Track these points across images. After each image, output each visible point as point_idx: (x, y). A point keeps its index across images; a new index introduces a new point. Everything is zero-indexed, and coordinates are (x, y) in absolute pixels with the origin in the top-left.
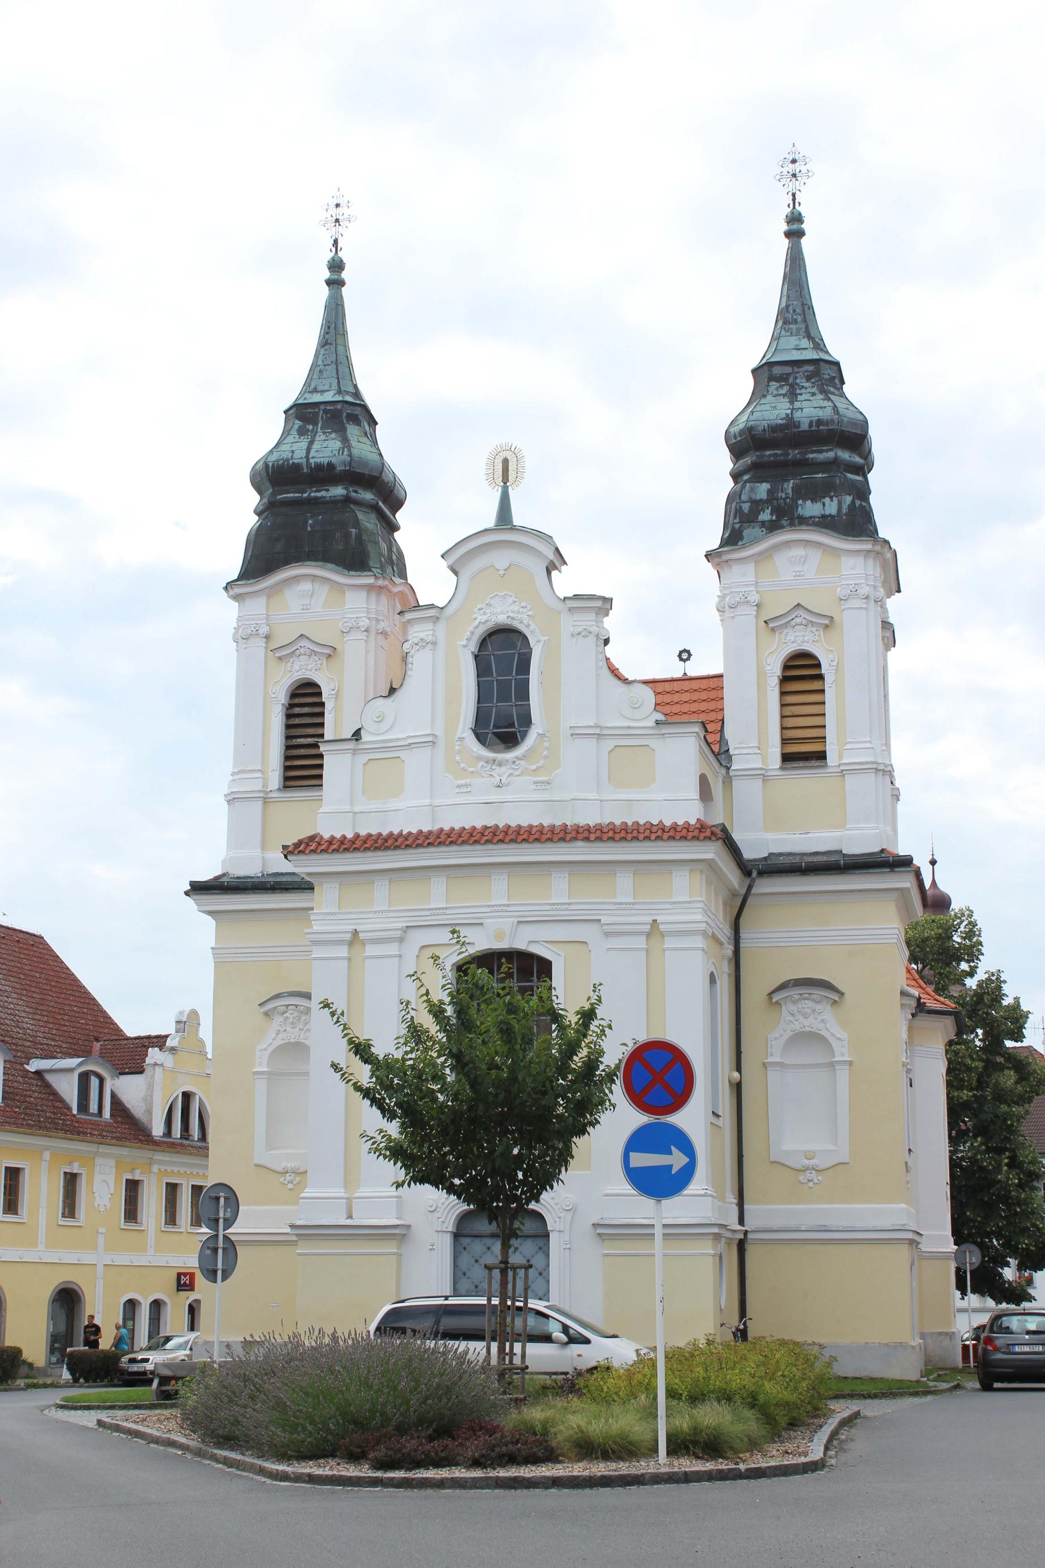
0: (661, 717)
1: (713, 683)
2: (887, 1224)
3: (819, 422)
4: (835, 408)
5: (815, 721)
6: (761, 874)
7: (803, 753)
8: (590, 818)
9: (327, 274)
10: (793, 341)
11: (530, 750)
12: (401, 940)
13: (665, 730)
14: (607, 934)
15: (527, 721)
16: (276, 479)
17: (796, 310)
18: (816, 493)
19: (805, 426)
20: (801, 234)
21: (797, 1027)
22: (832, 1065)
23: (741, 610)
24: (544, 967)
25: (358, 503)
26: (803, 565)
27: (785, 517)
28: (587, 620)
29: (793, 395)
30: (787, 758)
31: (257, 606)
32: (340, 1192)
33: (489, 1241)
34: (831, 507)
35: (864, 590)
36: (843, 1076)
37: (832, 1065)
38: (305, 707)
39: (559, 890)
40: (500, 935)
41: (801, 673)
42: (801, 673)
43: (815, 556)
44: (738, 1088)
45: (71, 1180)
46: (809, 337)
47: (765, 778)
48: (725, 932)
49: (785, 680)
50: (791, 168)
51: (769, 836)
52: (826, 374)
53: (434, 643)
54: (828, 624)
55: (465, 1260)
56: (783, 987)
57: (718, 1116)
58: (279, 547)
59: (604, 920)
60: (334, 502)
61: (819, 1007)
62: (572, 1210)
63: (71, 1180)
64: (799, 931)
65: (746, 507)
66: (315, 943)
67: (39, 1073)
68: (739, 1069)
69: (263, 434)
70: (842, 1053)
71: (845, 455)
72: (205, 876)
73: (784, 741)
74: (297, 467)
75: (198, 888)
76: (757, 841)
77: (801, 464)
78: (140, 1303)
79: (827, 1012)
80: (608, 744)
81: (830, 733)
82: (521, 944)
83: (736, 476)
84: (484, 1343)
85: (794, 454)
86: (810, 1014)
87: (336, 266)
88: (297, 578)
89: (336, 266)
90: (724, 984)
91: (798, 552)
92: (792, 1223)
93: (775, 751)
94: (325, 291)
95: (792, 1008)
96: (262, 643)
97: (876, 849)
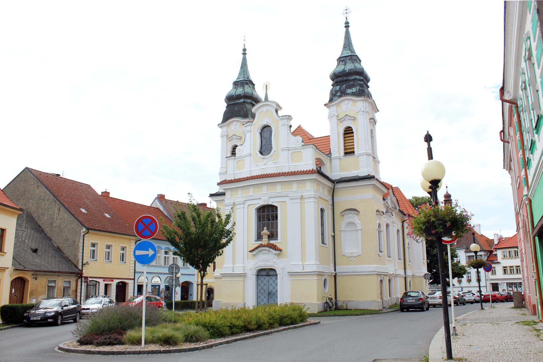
0: (303, 144)
1: (328, 138)
2: (371, 270)
3: (351, 70)
4: (355, 66)
5: (352, 144)
6: (337, 183)
7: (349, 152)
8: (286, 170)
9: (243, 52)
10: (346, 52)
11: (272, 155)
12: (244, 204)
13: (304, 147)
14: (291, 199)
15: (272, 148)
16: (230, 99)
17: (348, 44)
18: (350, 87)
19: (347, 71)
20: (348, 26)
21: (348, 221)
22: (357, 230)
23: (333, 118)
24: (276, 207)
25: (247, 103)
26: (351, 105)
27: (343, 93)
28: (285, 122)
29: (345, 64)
30: (346, 153)
31: (225, 129)
32: (231, 265)
33: (265, 277)
34: (354, 90)
35: (363, 110)
36: (360, 233)
37: (357, 230)
39: (279, 189)
40: (265, 201)
41: (348, 132)
42: (348, 132)
43: (351, 103)
44: (334, 237)
46: (350, 50)
47: (340, 159)
48: (329, 198)
49: (345, 134)
50: (346, 11)
51: (341, 173)
52: (354, 58)
53: (251, 131)
54: (354, 119)
55: (260, 281)
56: (344, 211)
57: (382, 252)
58: (229, 115)
59: (290, 195)
60: (241, 103)
61: (353, 216)
62: (283, 269)
64: (348, 197)
65: (334, 92)
66: (226, 206)
68: (334, 232)
69: (228, 88)
70: (359, 227)
71: (358, 77)
72: (214, 192)
73: (345, 149)
74: (233, 96)
76: (335, 175)
77: (350, 80)
78: (28, 281)
79: (356, 217)
80: (291, 152)
81: (355, 146)
82: (270, 203)
83: (333, 85)
85: (345, 78)
86: (351, 217)
87: (245, 50)
88: (233, 121)
89: (245, 50)
91: (346, 102)
92: (347, 270)
93: (342, 152)
94: (242, 56)
95: (347, 216)
96: (226, 137)
97: (367, 174)
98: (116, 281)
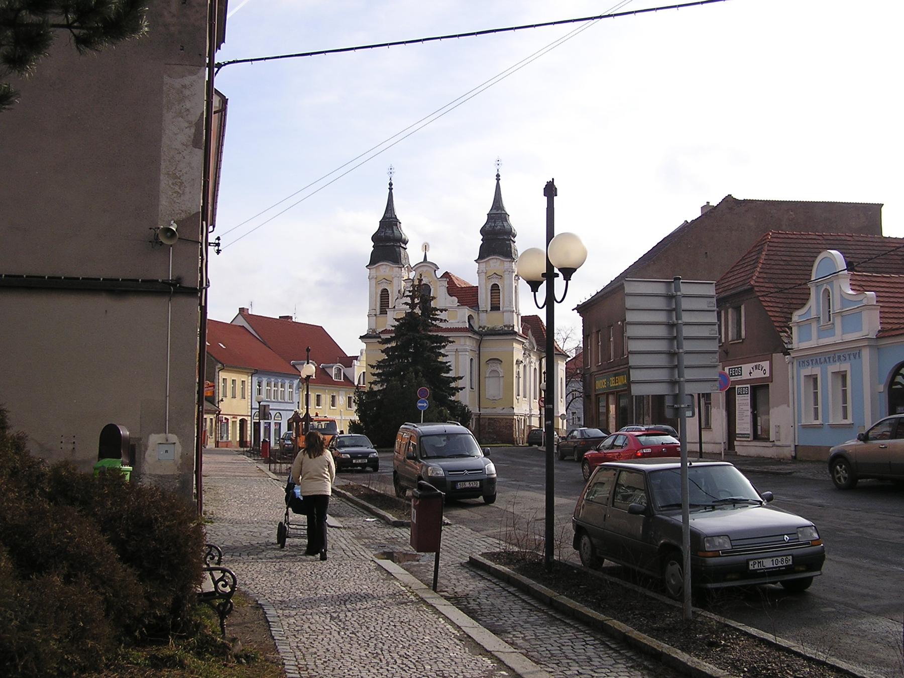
7: (495, 307)
26: (496, 264)
29: (495, 222)
38: (385, 294)
41: (495, 289)
42: (495, 289)
45: (333, 397)
48: (477, 348)
52: (504, 217)
63: (333, 397)
67: (294, 366)
75: (361, 337)
84: (276, 541)
87: (391, 184)
89: (391, 184)
90: (475, 362)
98: (240, 418)
